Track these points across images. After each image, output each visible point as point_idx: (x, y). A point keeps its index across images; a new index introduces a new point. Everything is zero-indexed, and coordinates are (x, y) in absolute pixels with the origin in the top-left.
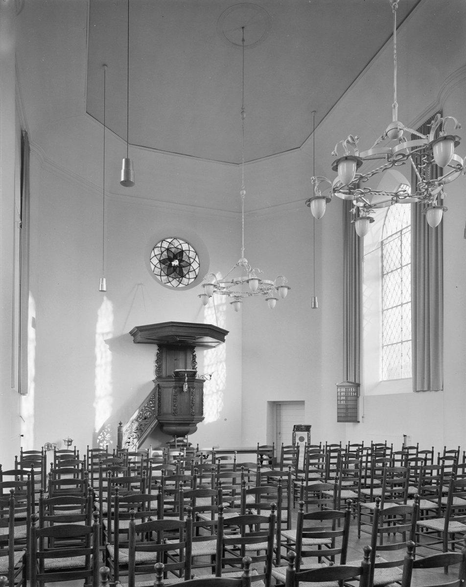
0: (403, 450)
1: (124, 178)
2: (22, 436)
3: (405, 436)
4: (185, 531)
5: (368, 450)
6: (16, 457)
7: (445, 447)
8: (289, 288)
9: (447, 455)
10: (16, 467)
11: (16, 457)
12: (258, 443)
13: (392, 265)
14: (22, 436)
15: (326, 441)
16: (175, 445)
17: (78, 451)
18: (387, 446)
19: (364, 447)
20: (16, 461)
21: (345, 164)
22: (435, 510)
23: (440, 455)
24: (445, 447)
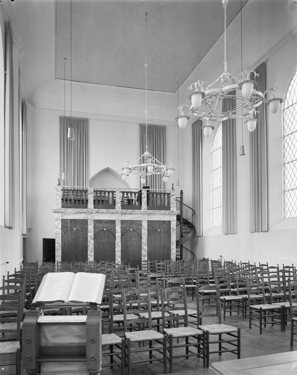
0: (284, 269)
1: (70, 136)
2: (8, 263)
3: (221, 256)
4: (256, 338)
5: (289, 268)
6: (4, 276)
7: (283, 265)
8: (173, 170)
9: (10, 278)
10: (4, 284)
11: (4, 276)
12: (259, 263)
13: (292, 157)
14: (8, 263)
15: (267, 262)
16: (162, 266)
17: (295, 267)
18: (250, 264)
19: (269, 266)
20: (4, 280)
21: (181, 119)
22: (197, 336)
23: (5, 277)
24: (283, 265)
